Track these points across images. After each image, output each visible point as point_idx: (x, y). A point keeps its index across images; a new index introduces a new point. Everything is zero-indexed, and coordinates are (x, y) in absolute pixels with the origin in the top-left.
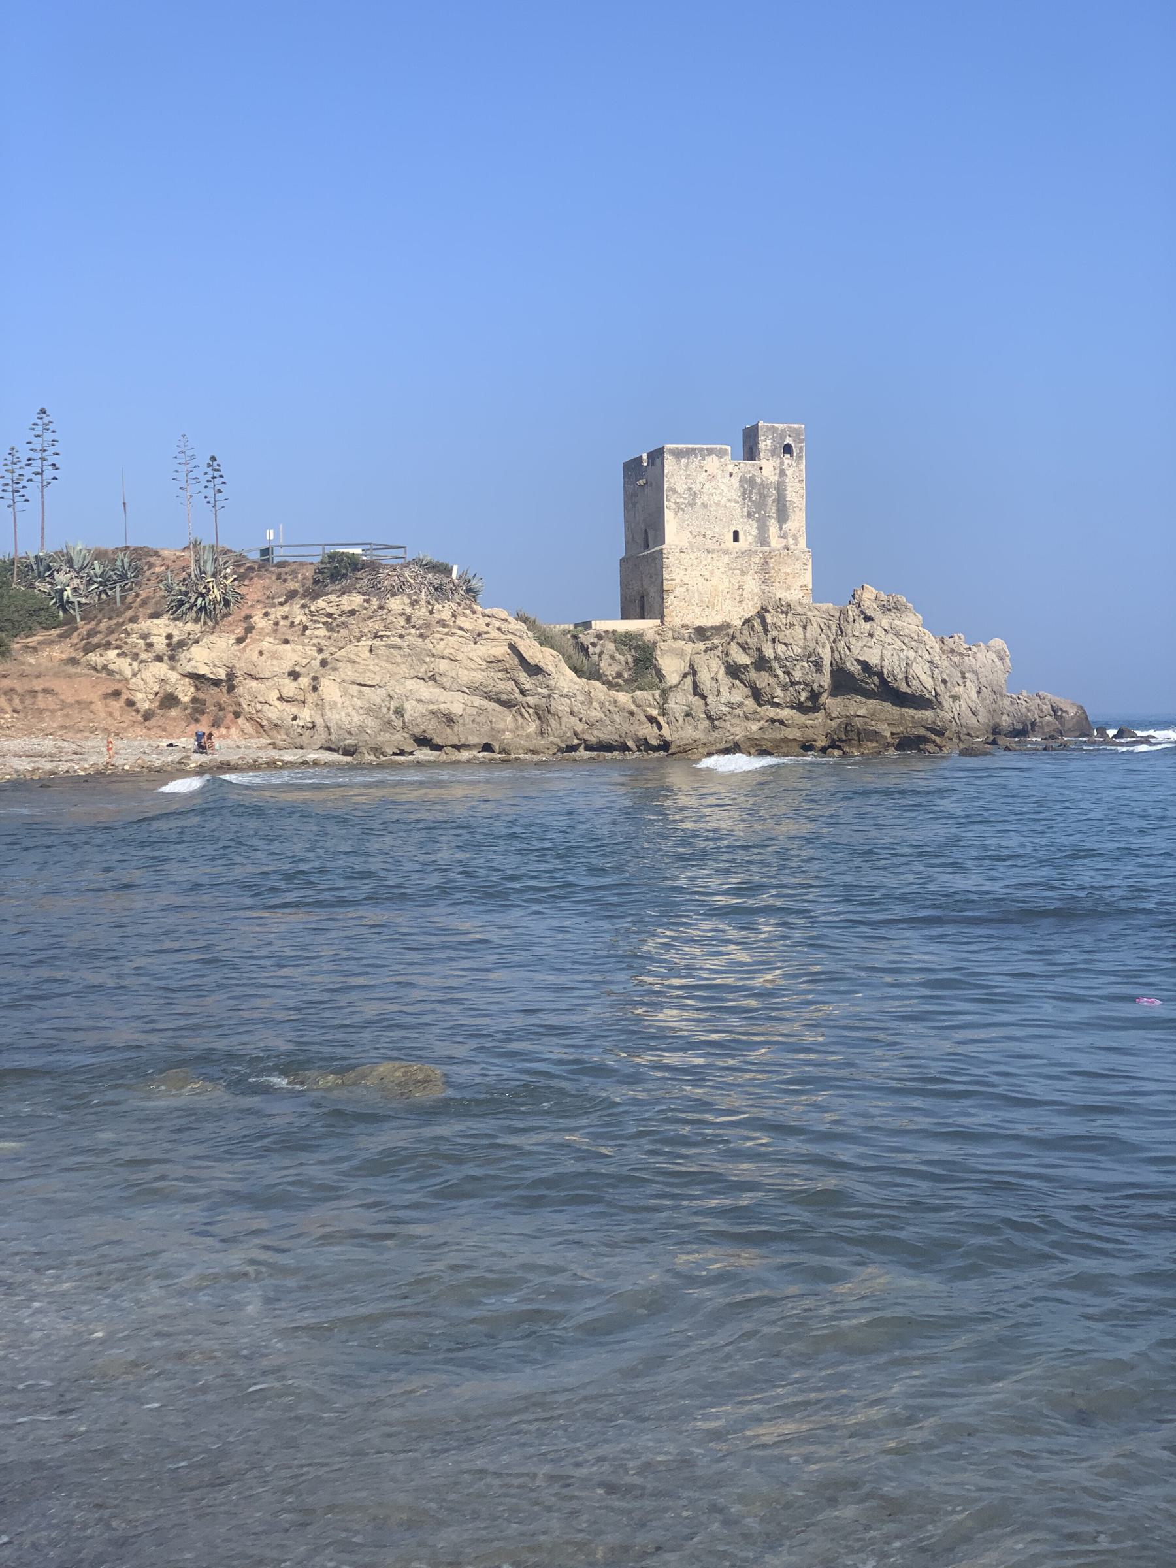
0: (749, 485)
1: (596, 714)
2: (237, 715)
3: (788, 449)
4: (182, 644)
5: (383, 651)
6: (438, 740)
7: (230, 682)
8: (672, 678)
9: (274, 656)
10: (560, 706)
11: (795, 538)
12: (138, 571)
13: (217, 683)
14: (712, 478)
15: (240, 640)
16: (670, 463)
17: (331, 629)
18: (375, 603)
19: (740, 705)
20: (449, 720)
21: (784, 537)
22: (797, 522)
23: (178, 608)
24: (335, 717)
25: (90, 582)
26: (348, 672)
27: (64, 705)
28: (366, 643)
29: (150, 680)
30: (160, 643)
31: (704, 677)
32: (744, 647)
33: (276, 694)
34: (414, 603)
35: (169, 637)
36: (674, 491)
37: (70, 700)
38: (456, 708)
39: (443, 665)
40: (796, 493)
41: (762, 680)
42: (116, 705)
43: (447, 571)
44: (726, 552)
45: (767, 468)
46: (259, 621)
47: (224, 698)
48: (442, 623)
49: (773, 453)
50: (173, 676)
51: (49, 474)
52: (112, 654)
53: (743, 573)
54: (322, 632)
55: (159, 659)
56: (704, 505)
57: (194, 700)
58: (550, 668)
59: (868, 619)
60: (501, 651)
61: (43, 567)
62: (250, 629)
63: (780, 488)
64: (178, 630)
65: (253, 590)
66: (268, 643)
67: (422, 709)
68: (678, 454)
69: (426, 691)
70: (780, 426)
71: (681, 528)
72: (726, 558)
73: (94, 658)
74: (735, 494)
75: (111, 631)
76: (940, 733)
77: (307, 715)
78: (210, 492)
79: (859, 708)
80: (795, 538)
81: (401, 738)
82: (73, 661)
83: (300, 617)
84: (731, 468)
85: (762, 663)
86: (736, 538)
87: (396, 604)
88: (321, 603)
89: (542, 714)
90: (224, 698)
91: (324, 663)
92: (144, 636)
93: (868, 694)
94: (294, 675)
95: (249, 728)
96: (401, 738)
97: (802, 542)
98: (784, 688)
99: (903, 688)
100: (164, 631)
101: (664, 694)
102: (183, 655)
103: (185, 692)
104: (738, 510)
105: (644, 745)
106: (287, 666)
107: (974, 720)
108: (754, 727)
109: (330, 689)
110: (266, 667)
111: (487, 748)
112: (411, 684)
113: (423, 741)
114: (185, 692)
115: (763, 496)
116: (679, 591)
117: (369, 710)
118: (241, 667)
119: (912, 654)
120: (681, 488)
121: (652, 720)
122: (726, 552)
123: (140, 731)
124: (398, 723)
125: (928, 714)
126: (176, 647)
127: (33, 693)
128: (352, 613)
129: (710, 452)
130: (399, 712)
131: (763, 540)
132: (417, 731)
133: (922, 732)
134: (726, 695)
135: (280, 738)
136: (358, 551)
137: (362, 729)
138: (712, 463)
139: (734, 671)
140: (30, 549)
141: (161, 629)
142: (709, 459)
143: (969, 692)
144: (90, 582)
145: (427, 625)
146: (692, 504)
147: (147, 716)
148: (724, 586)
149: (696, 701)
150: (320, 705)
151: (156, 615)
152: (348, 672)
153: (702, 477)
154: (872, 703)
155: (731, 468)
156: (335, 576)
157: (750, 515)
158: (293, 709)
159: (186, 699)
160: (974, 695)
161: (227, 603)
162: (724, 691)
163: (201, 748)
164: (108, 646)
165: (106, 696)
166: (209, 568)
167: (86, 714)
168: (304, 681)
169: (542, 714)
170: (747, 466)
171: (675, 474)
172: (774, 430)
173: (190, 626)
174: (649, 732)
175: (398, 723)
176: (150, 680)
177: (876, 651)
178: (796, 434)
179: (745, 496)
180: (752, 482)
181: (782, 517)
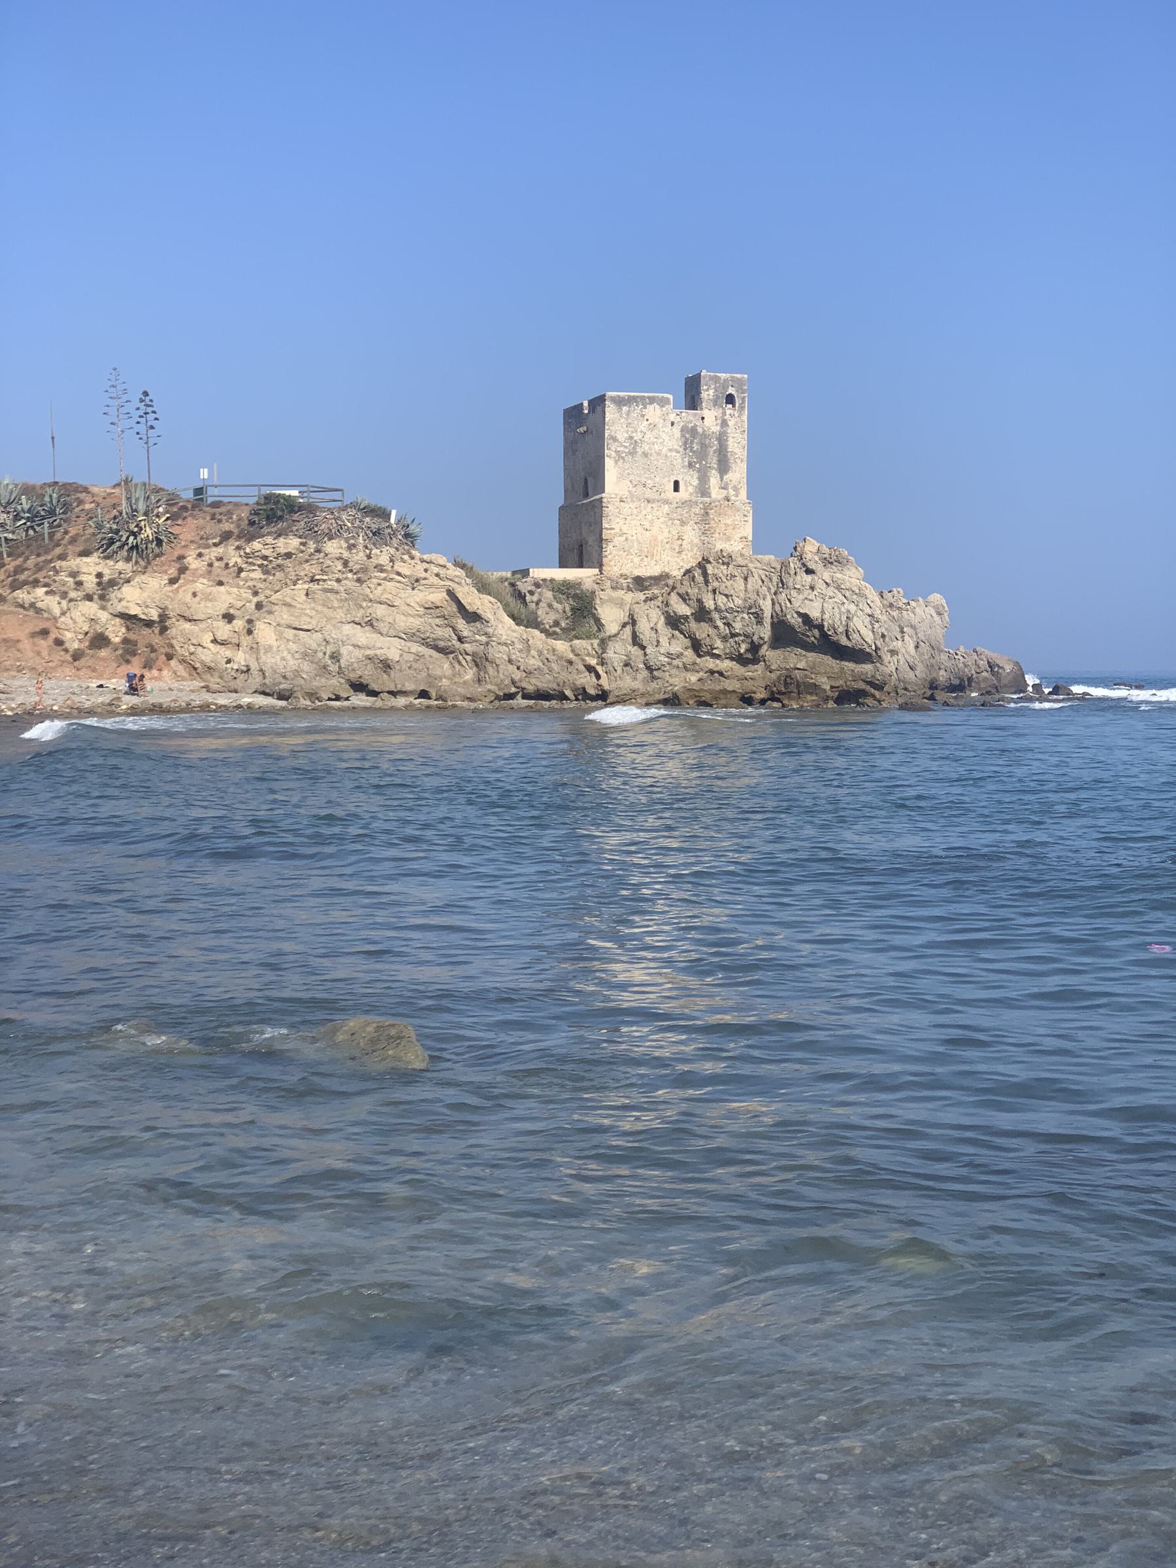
0: (690, 434)
1: (534, 662)
2: (169, 657)
3: (730, 399)
4: (112, 583)
5: (320, 595)
6: (374, 686)
7: (162, 624)
8: (612, 628)
9: (208, 598)
10: (499, 654)
11: (736, 489)
12: (67, 507)
13: (149, 624)
15: (172, 581)
16: (611, 411)
18: (312, 546)
19: (680, 656)
22: (738, 473)
23: (108, 546)
24: (270, 661)
25: (17, 517)
28: (302, 586)
29: (80, 620)
30: (90, 582)
31: (644, 627)
34: (351, 547)
35: (99, 575)
36: (615, 439)
38: (393, 654)
39: (380, 611)
40: (737, 444)
41: (702, 631)
42: (44, 644)
43: (386, 515)
44: (667, 502)
45: (710, 417)
46: (192, 562)
47: (156, 640)
48: (380, 568)
49: (715, 403)
50: (104, 616)
52: (40, 591)
53: (683, 523)
54: (258, 574)
55: (89, 598)
56: (645, 455)
57: (126, 641)
58: (488, 614)
60: (439, 597)
62: (183, 570)
63: (722, 438)
64: (108, 569)
65: (187, 530)
66: (201, 585)
67: (358, 654)
68: (619, 402)
69: (363, 636)
70: (723, 376)
71: (621, 477)
72: (666, 508)
73: (22, 595)
74: (677, 444)
76: (879, 688)
77: (241, 658)
78: (142, 428)
79: (798, 660)
80: (736, 489)
81: (337, 684)
83: (235, 559)
84: (672, 417)
85: (702, 614)
87: (333, 547)
88: (256, 545)
89: (480, 662)
90: (156, 640)
91: (259, 606)
92: (74, 574)
94: (229, 618)
95: (181, 670)
96: (337, 684)
98: (724, 639)
99: (844, 641)
100: (95, 570)
103: (116, 632)
104: (678, 460)
106: (222, 608)
108: (694, 678)
109: (265, 633)
110: (200, 609)
112: (348, 629)
114: (116, 632)
115: (704, 447)
116: (618, 541)
117: (305, 655)
118: (174, 609)
119: (852, 608)
120: (622, 436)
122: (667, 502)
124: (333, 668)
125: (868, 668)
126: (106, 587)
128: (288, 555)
129: (652, 400)
130: (335, 657)
131: (703, 491)
132: (352, 676)
135: (214, 681)
136: (294, 493)
137: (297, 673)
138: (653, 412)
139: (674, 622)
141: (91, 567)
142: (650, 408)
144: (17, 517)
145: (364, 570)
146: (632, 453)
147: (77, 656)
150: (254, 649)
151: (86, 553)
152: (285, 616)
153: (643, 425)
154: (812, 656)
155: (672, 417)
156: (271, 518)
158: (227, 652)
162: (664, 641)
164: (36, 583)
165: (33, 635)
168: (239, 624)
169: (480, 662)
170: (689, 416)
171: (616, 421)
172: (717, 379)
173: (121, 565)
175: (333, 668)
176: (80, 620)
177: (817, 604)
178: (738, 384)
179: (687, 445)
180: (693, 431)
181: (724, 467)
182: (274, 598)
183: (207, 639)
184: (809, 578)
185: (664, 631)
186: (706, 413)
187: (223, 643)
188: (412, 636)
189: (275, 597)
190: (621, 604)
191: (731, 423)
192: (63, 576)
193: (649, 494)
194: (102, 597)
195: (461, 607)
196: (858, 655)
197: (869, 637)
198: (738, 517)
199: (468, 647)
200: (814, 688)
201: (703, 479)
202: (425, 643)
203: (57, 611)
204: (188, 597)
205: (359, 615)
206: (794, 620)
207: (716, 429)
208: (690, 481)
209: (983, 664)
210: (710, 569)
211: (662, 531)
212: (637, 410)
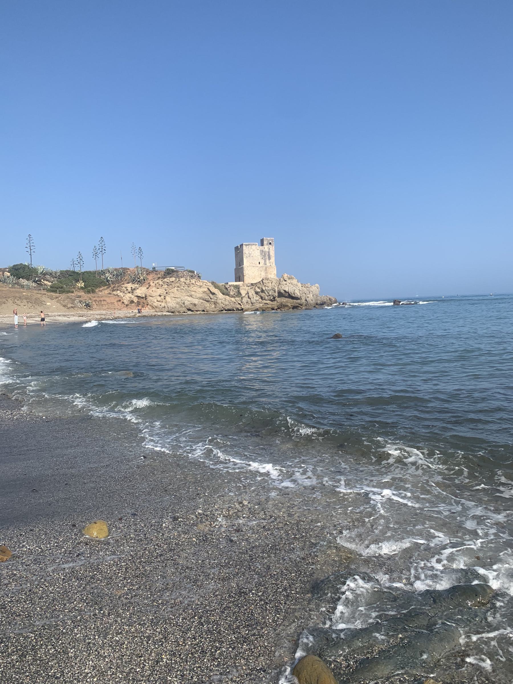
1: (227, 303)
2: (147, 305)
3: (270, 244)
4: (134, 289)
5: (180, 290)
6: (192, 310)
7: (146, 298)
8: (243, 295)
9: (155, 292)
10: (219, 301)
11: (272, 263)
13: (143, 298)
15: (147, 288)
17: (168, 285)
18: (178, 279)
19: (258, 300)
20: (195, 305)
22: (273, 259)
23: (133, 281)
24: (169, 305)
25: (114, 276)
27: (108, 303)
28: (176, 288)
29: (127, 297)
30: (129, 289)
31: (250, 294)
32: (259, 288)
34: (186, 279)
35: (131, 288)
36: (245, 253)
37: (109, 302)
38: (196, 303)
39: (193, 293)
40: (272, 253)
41: (263, 295)
42: (120, 303)
43: (194, 272)
45: (266, 248)
46: (151, 284)
47: (145, 301)
48: (193, 284)
49: (267, 244)
50: (133, 296)
51: (103, 252)
52: (119, 292)
53: (261, 271)
54: (166, 286)
55: (129, 293)
56: (252, 256)
57: (138, 302)
59: (285, 281)
60: (206, 290)
61: (103, 273)
62: (150, 286)
63: (269, 252)
64: (134, 286)
65: (150, 277)
66: (154, 289)
67: (189, 303)
68: (246, 245)
69: (190, 299)
70: (268, 238)
73: (115, 293)
74: (259, 254)
75: (118, 286)
77: (163, 304)
78: (139, 255)
79: (284, 300)
80: (272, 263)
81: (184, 309)
82: (110, 294)
83: (161, 283)
85: (263, 291)
87: (182, 280)
88: (165, 280)
89: (215, 303)
90: (145, 301)
91: (167, 293)
92: (126, 288)
94: (160, 296)
95: (150, 308)
98: (268, 296)
99: (293, 295)
101: (242, 298)
103: (136, 300)
105: (237, 309)
107: (312, 302)
108: (261, 305)
109: (168, 299)
110: (154, 294)
111: (203, 311)
112: (186, 297)
113: (189, 310)
114: (136, 300)
115: (265, 254)
116: (247, 276)
118: (148, 294)
119: (295, 288)
120: (247, 253)
121: (239, 304)
123: (126, 309)
124: (183, 306)
125: (299, 301)
126: (133, 290)
127: (101, 301)
128: (173, 282)
129: (253, 244)
130: (184, 303)
133: (298, 305)
134: (255, 298)
135: (157, 310)
136: (173, 268)
137: (176, 307)
138: (254, 247)
139: (257, 293)
140: (100, 268)
141: (130, 286)
145: (189, 284)
146: (250, 256)
149: (249, 299)
151: (128, 283)
152: (172, 295)
153: (252, 250)
158: (160, 303)
159: (136, 301)
162: (255, 297)
163: (139, 312)
164: (118, 290)
165: (117, 301)
167: (113, 305)
168: (162, 297)
169: (215, 303)
171: (245, 249)
172: (267, 239)
173: (136, 285)
174: (239, 307)
175: (183, 306)
176: (127, 297)
177: (287, 288)
178: (272, 240)
180: (263, 251)
181: (269, 259)
183: (155, 300)
184: (285, 282)
186: (265, 247)
187: (159, 301)
193: (254, 265)
194: (132, 292)
196: (297, 298)
197: (299, 294)
199: (213, 300)
201: (265, 261)
202: (203, 300)
203: (122, 296)
204: (151, 292)
206: (283, 292)
207: (268, 250)
208: (262, 262)
209: (328, 299)
210: (264, 281)
212: (250, 247)
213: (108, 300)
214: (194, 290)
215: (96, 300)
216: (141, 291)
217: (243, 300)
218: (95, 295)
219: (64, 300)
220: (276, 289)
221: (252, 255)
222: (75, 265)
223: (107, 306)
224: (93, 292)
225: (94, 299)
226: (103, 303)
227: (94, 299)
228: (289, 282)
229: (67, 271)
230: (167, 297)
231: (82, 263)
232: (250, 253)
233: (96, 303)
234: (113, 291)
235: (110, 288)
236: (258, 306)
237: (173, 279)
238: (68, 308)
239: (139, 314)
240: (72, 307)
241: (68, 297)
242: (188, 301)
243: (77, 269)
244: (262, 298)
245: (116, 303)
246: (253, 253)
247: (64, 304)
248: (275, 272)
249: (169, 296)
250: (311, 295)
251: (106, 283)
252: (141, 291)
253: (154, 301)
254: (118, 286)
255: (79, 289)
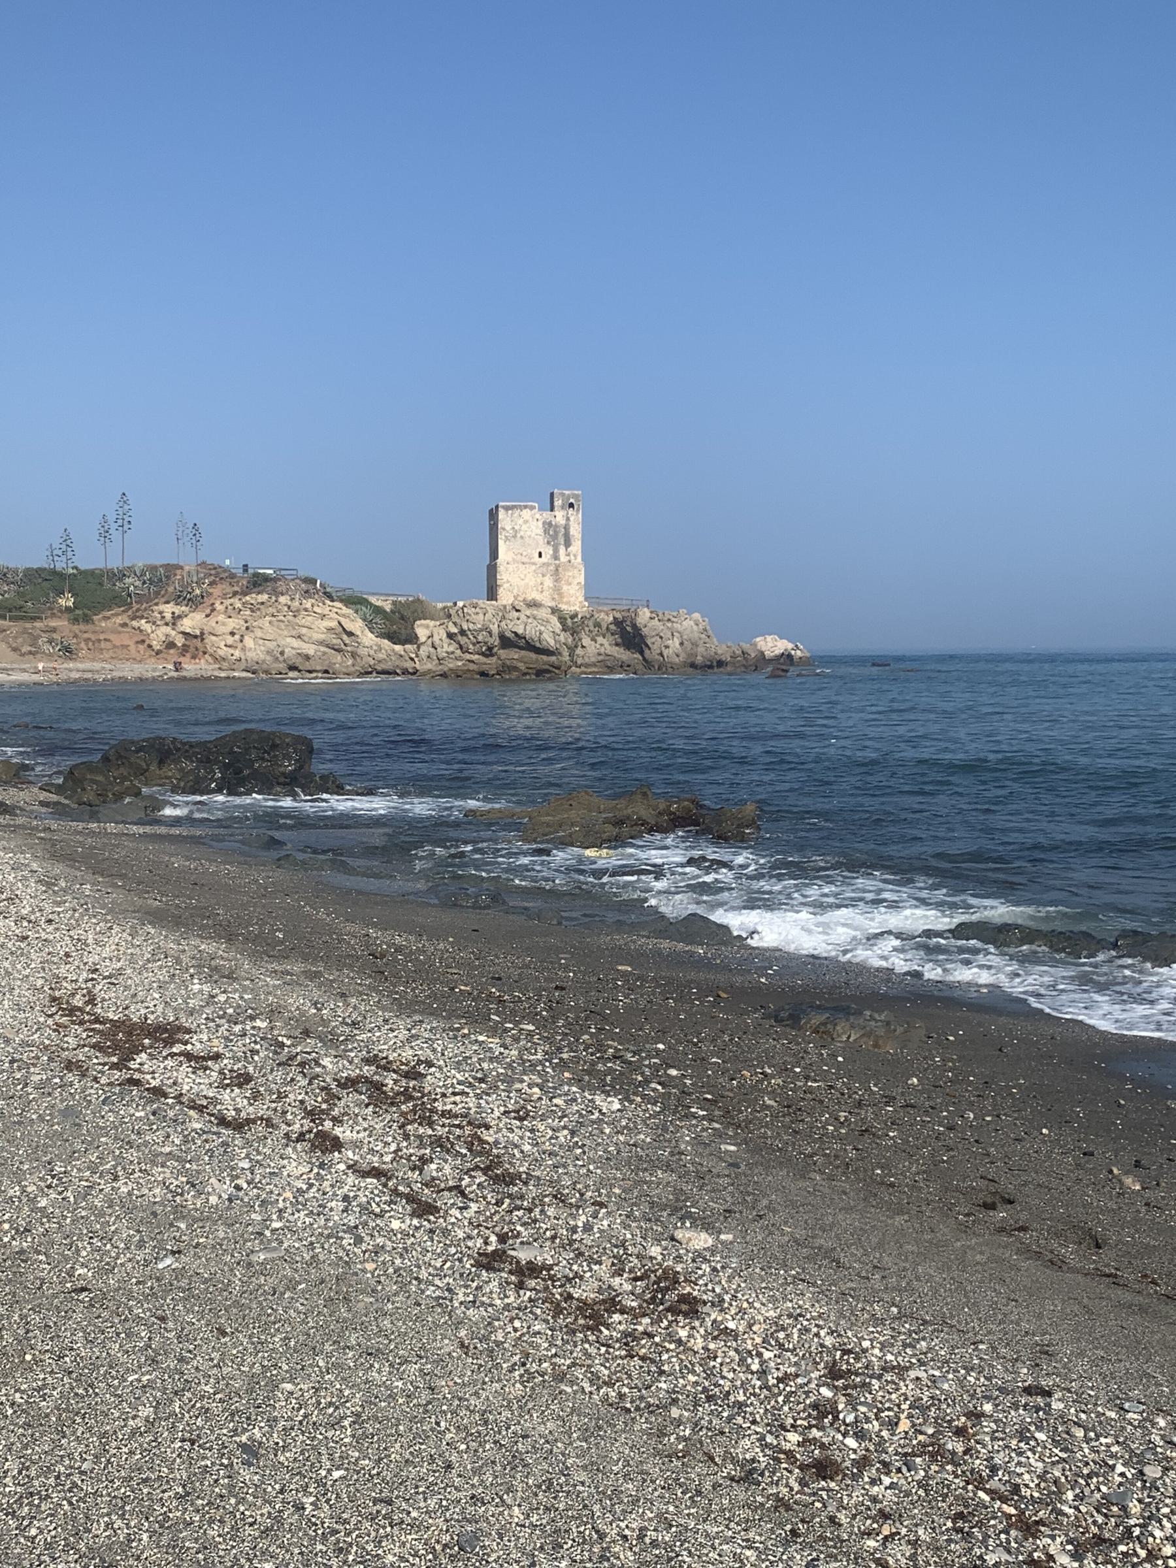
0: (548, 526)
1: (382, 656)
2: (205, 653)
3: (571, 505)
4: (180, 617)
5: (276, 623)
6: (301, 668)
7: (202, 637)
8: (422, 639)
9: (224, 624)
10: (362, 651)
11: (575, 556)
12: (168, 577)
13: (196, 637)
14: (526, 522)
15: (207, 616)
16: (502, 514)
17: (253, 611)
18: (274, 598)
19: (453, 653)
20: (307, 658)
21: (568, 555)
22: (576, 547)
23: (178, 599)
24: (251, 655)
25: (144, 583)
26: (259, 633)
27: (115, 646)
28: (268, 618)
29: (161, 635)
30: (168, 616)
31: (436, 638)
32: (455, 624)
33: (223, 643)
34: (292, 599)
35: (173, 613)
36: (504, 529)
37: (118, 644)
38: (311, 652)
39: (304, 631)
40: (576, 531)
41: (463, 640)
42: (141, 647)
43: (314, 582)
44: (534, 564)
45: (559, 516)
46: (218, 606)
47: (199, 644)
48: (306, 610)
49: (563, 508)
50: (173, 633)
51: (126, 526)
52: (143, 621)
53: (543, 576)
54: (248, 612)
55: (167, 624)
56: (522, 537)
57: (184, 645)
58: (358, 633)
59: (518, 611)
60: (334, 624)
61: (122, 575)
62: (213, 610)
63: (567, 528)
64: (178, 610)
65: (216, 591)
66: (221, 618)
67: (294, 652)
68: (507, 508)
69: (296, 643)
70: (567, 492)
71: (508, 550)
72: (534, 567)
73: (135, 623)
74: (540, 531)
75: (145, 609)
76: (558, 668)
77: (237, 654)
78: (194, 541)
79: (514, 654)
80: (575, 556)
81: (282, 666)
82: (125, 625)
83: (238, 605)
84: (538, 516)
85: (463, 632)
86: (540, 555)
87: (282, 599)
88: (248, 598)
89: (354, 655)
90: (199, 644)
91: (247, 628)
92: (161, 613)
93: (521, 648)
94: (232, 634)
95: (210, 660)
96: (282, 666)
97: (579, 559)
98: (474, 644)
99: (538, 645)
100: (170, 611)
101: (419, 648)
102: (179, 624)
103: (180, 641)
104: (541, 540)
105: (405, 672)
106: (229, 629)
107: (677, 660)
108: (460, 663)
109: (249, 642)
110: (220, 629)
111: (326, 672)
112: (289, 640)
113: (293, 668)
114: (180, 641)
115: (556, 533)
116: (506, 586)
117: (268, 652)
118: (207, 629)
119: (543, 628)
120: (508, 528)
121: (412, 659)
122: (534, 564)
123: (153, 660)
124: (281, 659)
125: (553, 658)
126: (176, 618)
127: (99, 641)
128: (263, 603)
129: (526, 507)
130: (282, 653)
131: (556, 557)
132: (290, 663)
133: (547, 667)
134: (446, 648)
135: (225, 665)
136: (271, 572)
137: (264, 661)
138: (526, 513)
139: (450, 636)
140: (115, 563)
141: (169, 609)
142: (525, 511)
143: (675, 644)
144: (144, 583)
145: (298, 611)
146: (515, 537)
147: (158, 653)
148: (532, 583)
149: (432, 650)
150: (243, 649)
151: (167, 602)
152: (259, 633)
153: (520, 521)
154: (523, 652)
155: (538, 516)
156: (255, 584)
157: (548, 543)
158: (231, 651)
159: (180, 645)
160: (677, 645)
161: (203, 597)
162: (445, 646)
163: (177, 670)
164: (142, 617)
165: (137, 642)
166: (195, 579)
167: (125, 651)
168: (237, 637)
169: (354, 655)
170: (547, 515)
171: (505, 520)
172: (563, 494)
173: (183, 608)
174: (409, 665)
175: (281, 659)
176: (161, 635)
177: (522, 627)
178: (576, 497)
179: (546, 532)
180: (550, 524)
181: (568, 544)
182: (255, 624)
183: (222, 644)
184: (516, 614)
185: (446, 640)
186: (556, 513)
187: (230, 646)
188: (321, 643)
189: (255, 624)
190: (427, 627)
191: (572, 519)
192: (156, 614)
193: (525, 560)
194: (174, 624)
195: (344, 629)
196: (547, 652)
197: (552, 643)
198: (576, 571)
199: (349, 649)
200: (516, 668)
201: (556, 551)
202: (327, 646)
203: (149, 631)
204: (214, 624)
205: (294, 633)
206: (508, 634)
207: (563, 522)
208: (548, 551)
209: (739, 652)
210: (466, 610)
211: (531, 580)
212: (517, 512)
213: (116, 640)
214: (307, 624)
215: (89, 639)
216: (192, 622)
217: (421, 652)
218: (90, 627)
219: (15, 637)
220: (495, 629)
221: (522, 533)
222: (56, 558)
223: (111, 653)
224: (87, 620)
225: (86, 636)
226: (103, 645)
227: (86, 636)
228: (528, 613)
229: (39, 571)
230: (246, 637)
231: (70, 554)
232: (517, 528)
233: (87, 644)
234: (133, 619)
235: (130, 613)
236: (452, 664)
237: (264, 597)
238: (23, 655)
239: (175, 674)
240: (30, 653)
241: (25, 632)
242: (292, 646)
243: (59, 566)
244: (461, 647)
245: (133, 647)
246: (524, 527)
247: (14, 645)
248: (582, 579)
249: (252, 634)
250: (677, 642)
251: (121, 600)
252: (192, 622)
253: (220, 645)
254: (145, 609)
255: (61, 611)
